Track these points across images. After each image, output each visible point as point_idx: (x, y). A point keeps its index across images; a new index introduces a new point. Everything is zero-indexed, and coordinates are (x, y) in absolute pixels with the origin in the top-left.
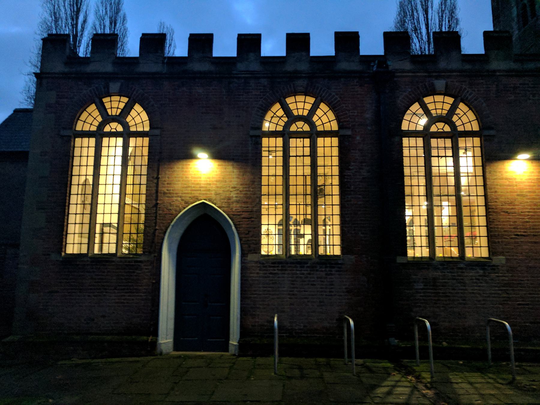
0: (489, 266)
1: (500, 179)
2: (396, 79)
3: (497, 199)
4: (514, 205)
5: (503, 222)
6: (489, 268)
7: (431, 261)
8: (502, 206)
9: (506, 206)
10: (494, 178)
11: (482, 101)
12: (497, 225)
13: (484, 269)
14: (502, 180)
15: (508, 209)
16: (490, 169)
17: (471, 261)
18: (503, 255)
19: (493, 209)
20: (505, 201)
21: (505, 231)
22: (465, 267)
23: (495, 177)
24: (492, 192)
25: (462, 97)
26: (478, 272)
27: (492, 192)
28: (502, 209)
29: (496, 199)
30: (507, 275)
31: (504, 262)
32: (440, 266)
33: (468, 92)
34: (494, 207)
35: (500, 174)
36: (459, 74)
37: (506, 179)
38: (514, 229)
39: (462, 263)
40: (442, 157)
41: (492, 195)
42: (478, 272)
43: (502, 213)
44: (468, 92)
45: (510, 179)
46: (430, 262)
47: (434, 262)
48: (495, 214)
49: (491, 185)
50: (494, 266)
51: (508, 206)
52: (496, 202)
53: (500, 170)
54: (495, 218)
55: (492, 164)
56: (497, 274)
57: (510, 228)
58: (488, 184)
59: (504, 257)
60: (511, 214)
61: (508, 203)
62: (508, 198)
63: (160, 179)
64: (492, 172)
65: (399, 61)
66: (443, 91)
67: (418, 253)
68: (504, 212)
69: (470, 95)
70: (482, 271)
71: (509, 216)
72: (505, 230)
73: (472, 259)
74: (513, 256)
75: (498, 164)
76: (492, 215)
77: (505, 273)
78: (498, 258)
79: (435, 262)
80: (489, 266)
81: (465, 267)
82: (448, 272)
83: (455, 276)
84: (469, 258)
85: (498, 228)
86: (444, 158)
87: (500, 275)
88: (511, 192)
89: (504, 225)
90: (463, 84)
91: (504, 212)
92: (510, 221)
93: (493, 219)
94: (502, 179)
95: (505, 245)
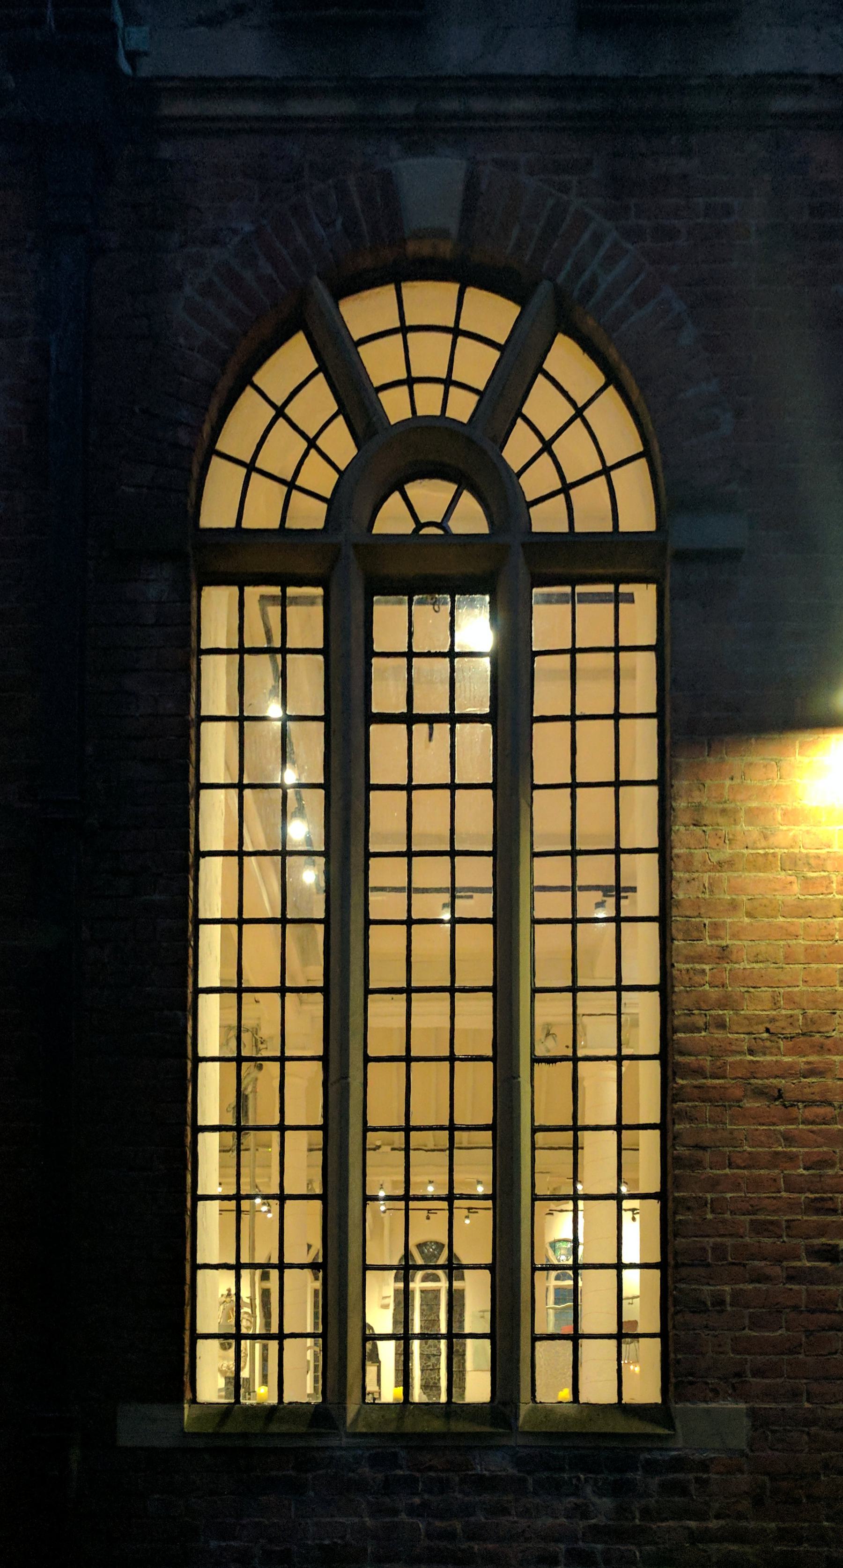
0: (651, 1467)
1: (754, 865)
2: (166, 151)
3: (725, 1003)
4: (821, 1049)
5: (753, 1162)
6: (654, 1482)
7: (319, 1435)
8: (751, 1052)
9: (779, 1052)
10: (715, 858)
11: (679, 306)
12: (714, 1184)
13: (620, 1489)
14: (765, 868)
15: (787, 1072)
16: (698, 797)
17: (549, 1435)
18: (738, 1393)
19: (699, 1072)
20: (773, 1020)
21: (760, 1228)
22: (512, 1471)
23: (727, 852)
24: (700, 959)
25: (561, 279)
26: (582, 1511)
27: (700, 959)
28: (754, 1071)
29: (723, 1007)
30: (752, 1525)
31: (739, 1440)
32: (366, 1470)
33: (597, 240)
34: (706, 1061)
35: (754, 832)
36: (548, 105)
37: (792, 863)
38: (818, 1211)
39: (499, 1448)
40: (431, 719)
41: (697, 979)
42: (582, 1511)
43: (748, 1104)
44: (597, 240)
45: (808, 862)
46: (315, 1443)
47: (334, 1442)
48: (707, 1110)
49: (697, 903)
50: (679, 1464)
51: (790, 1052)
52: (721, 1025)
53: (754, 804)
54: (706, 1139)
55: (711, 760)
56: (692, 1524)
57: (792, 1206)
58: (679, 903)
59: (742, 1406)
60: (801, 1112)
61: (788, 1031)
62: (791, 1000)
63: (258, 1094)
64: (707, 819)
65: (201, 22)
66: (442, 234)
67: (636, 1362)
68: (760, 1093)
69: (611, 260)
70: (606, 1503)
71: (793, 1121)
72: (761, 1217)
73: (566, 1418)
74: (795, 1395)
75: (749, 759)
76: (691, 1119)
77: (740, 1516)
78: (708, 1411)
79: (345, 1441)
80: (651, 1467)
81: (512, 1471)
82: (412, 1511)
83: (451, 1536)
84: (548, 1412)
85: (716, 1206)
86: (442, 730)
87: (713, 1524)
88: (813, 955)
89: (756, 1184)
90: (564, 188)
91: (760, 1093)
92: (792, 1158)
93: (697, 1147)
94: (764, 862)
95: (756, 1323)
